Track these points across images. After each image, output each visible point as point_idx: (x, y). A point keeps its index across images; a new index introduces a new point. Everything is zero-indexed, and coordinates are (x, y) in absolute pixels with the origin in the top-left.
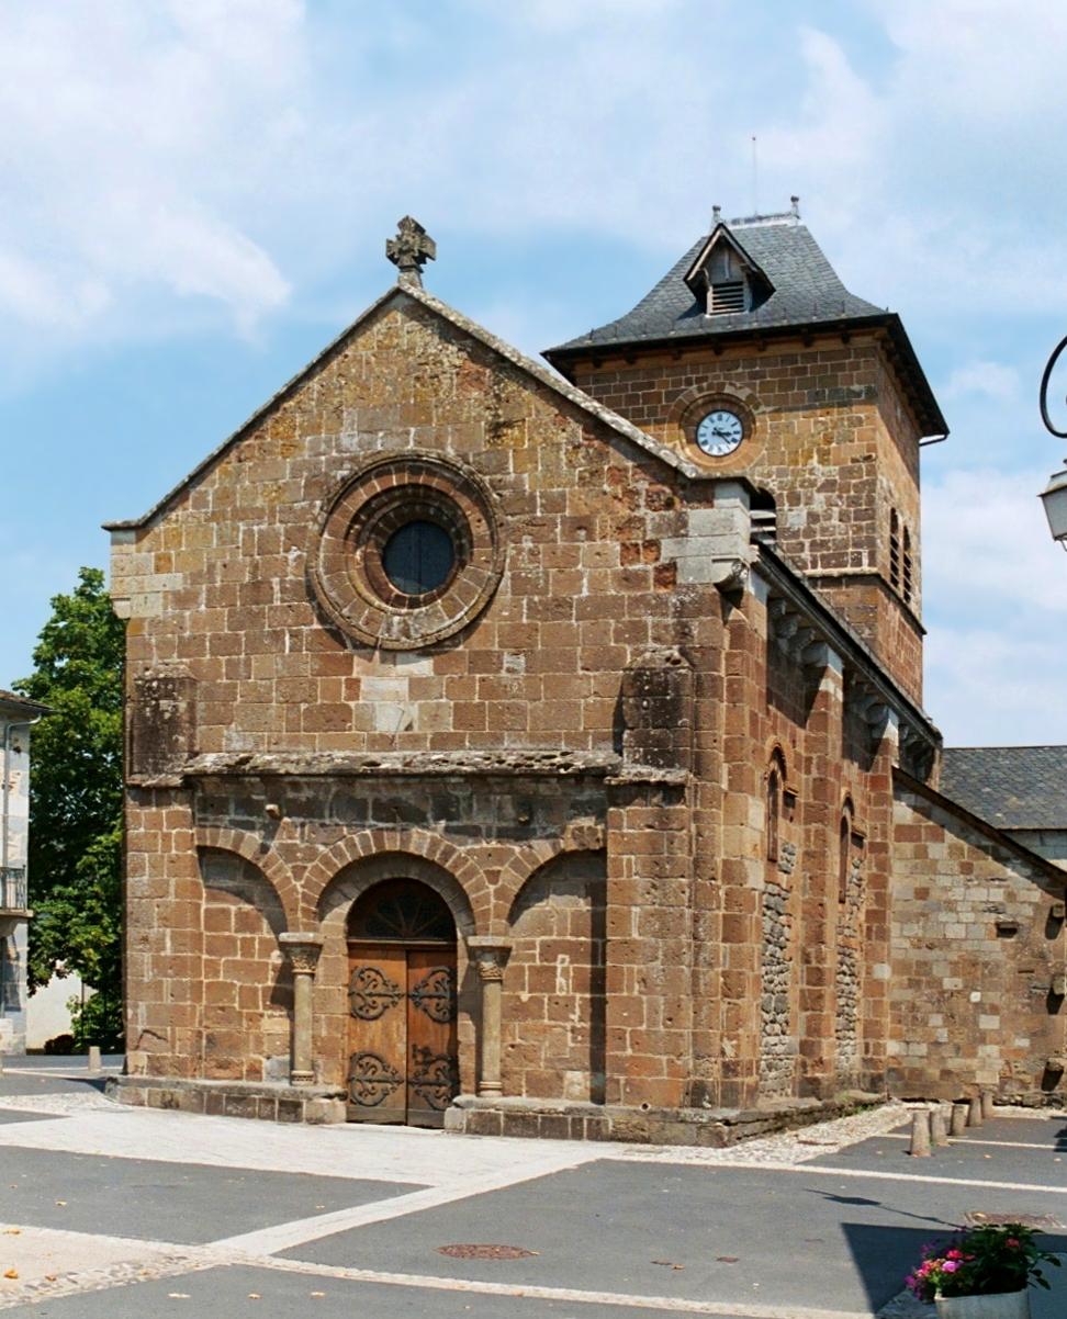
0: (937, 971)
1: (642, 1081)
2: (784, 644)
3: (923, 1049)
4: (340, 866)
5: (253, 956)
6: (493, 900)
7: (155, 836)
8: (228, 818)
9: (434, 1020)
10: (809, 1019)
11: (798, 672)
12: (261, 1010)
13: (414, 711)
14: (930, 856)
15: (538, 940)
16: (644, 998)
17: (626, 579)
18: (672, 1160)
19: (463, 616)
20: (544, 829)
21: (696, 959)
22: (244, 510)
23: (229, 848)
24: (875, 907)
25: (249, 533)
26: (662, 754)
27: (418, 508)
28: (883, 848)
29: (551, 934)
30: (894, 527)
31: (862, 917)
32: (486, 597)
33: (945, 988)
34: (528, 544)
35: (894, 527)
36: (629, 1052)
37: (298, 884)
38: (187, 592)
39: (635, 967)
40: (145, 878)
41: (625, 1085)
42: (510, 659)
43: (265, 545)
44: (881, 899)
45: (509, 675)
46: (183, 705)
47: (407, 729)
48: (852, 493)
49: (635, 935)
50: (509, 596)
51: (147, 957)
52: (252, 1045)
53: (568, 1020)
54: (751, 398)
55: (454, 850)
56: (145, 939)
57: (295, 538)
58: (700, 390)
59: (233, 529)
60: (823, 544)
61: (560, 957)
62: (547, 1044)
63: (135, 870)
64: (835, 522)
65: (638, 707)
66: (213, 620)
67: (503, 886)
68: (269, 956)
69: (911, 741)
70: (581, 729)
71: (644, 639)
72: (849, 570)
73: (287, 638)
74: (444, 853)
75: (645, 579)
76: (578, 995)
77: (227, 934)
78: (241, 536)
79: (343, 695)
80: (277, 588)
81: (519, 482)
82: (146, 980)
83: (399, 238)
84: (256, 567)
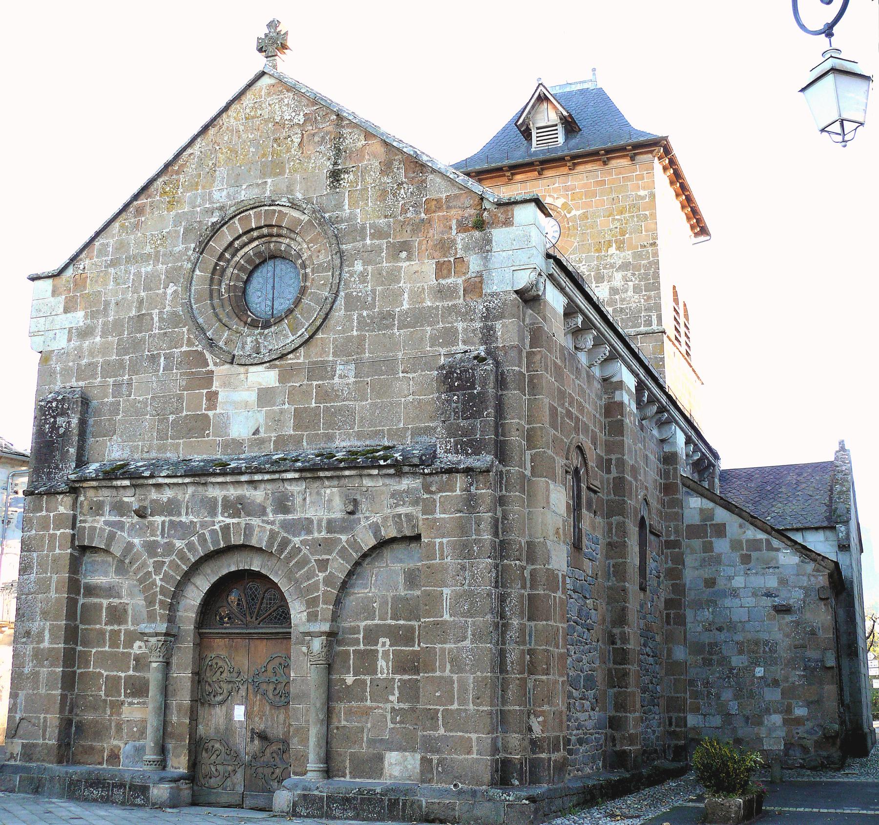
0: (726, 651)
3: (717, 721)
4: (193, 561)
6: (322, 587)
10: (616, 696)
11: (597, 385)
15: (362, 624)
19: (303, 332)
20: (367, 518)
21: (503, 638)
24: (673, 596)
25: (138, 274)
26: (470, 443)
27: (272, 245)
28: (676, 544)
30: (676, 301)
31: (662, 605)
32: (322, 314)
33: (733, 664)
34: (358, 267)
35: (676, 301)
36: (442, 731)
37: (158, 579)
38: (88, 327)
39: (447, 646)
41: (438, 764)
42: (341, 367)
43: (150, 283)
44: (679, 589)
46: (75, 421)
47: (254, 434)
48: (643, 271)
49: (447, 617)
50: (343, 312)
54: (565, 205)
55: (290, 541)
61: (381, 640)
62: (369, 725)
64: (630, 293)
66: (104, 350)
68: (132, 647)
69: (696, 458)
70: (401, 425)
71: (454, 343)
72: (643, 329)
77: (98, 626)
78: (132, 277)
80: (156, 319)
83: (266, 35)
84: (141, 302)
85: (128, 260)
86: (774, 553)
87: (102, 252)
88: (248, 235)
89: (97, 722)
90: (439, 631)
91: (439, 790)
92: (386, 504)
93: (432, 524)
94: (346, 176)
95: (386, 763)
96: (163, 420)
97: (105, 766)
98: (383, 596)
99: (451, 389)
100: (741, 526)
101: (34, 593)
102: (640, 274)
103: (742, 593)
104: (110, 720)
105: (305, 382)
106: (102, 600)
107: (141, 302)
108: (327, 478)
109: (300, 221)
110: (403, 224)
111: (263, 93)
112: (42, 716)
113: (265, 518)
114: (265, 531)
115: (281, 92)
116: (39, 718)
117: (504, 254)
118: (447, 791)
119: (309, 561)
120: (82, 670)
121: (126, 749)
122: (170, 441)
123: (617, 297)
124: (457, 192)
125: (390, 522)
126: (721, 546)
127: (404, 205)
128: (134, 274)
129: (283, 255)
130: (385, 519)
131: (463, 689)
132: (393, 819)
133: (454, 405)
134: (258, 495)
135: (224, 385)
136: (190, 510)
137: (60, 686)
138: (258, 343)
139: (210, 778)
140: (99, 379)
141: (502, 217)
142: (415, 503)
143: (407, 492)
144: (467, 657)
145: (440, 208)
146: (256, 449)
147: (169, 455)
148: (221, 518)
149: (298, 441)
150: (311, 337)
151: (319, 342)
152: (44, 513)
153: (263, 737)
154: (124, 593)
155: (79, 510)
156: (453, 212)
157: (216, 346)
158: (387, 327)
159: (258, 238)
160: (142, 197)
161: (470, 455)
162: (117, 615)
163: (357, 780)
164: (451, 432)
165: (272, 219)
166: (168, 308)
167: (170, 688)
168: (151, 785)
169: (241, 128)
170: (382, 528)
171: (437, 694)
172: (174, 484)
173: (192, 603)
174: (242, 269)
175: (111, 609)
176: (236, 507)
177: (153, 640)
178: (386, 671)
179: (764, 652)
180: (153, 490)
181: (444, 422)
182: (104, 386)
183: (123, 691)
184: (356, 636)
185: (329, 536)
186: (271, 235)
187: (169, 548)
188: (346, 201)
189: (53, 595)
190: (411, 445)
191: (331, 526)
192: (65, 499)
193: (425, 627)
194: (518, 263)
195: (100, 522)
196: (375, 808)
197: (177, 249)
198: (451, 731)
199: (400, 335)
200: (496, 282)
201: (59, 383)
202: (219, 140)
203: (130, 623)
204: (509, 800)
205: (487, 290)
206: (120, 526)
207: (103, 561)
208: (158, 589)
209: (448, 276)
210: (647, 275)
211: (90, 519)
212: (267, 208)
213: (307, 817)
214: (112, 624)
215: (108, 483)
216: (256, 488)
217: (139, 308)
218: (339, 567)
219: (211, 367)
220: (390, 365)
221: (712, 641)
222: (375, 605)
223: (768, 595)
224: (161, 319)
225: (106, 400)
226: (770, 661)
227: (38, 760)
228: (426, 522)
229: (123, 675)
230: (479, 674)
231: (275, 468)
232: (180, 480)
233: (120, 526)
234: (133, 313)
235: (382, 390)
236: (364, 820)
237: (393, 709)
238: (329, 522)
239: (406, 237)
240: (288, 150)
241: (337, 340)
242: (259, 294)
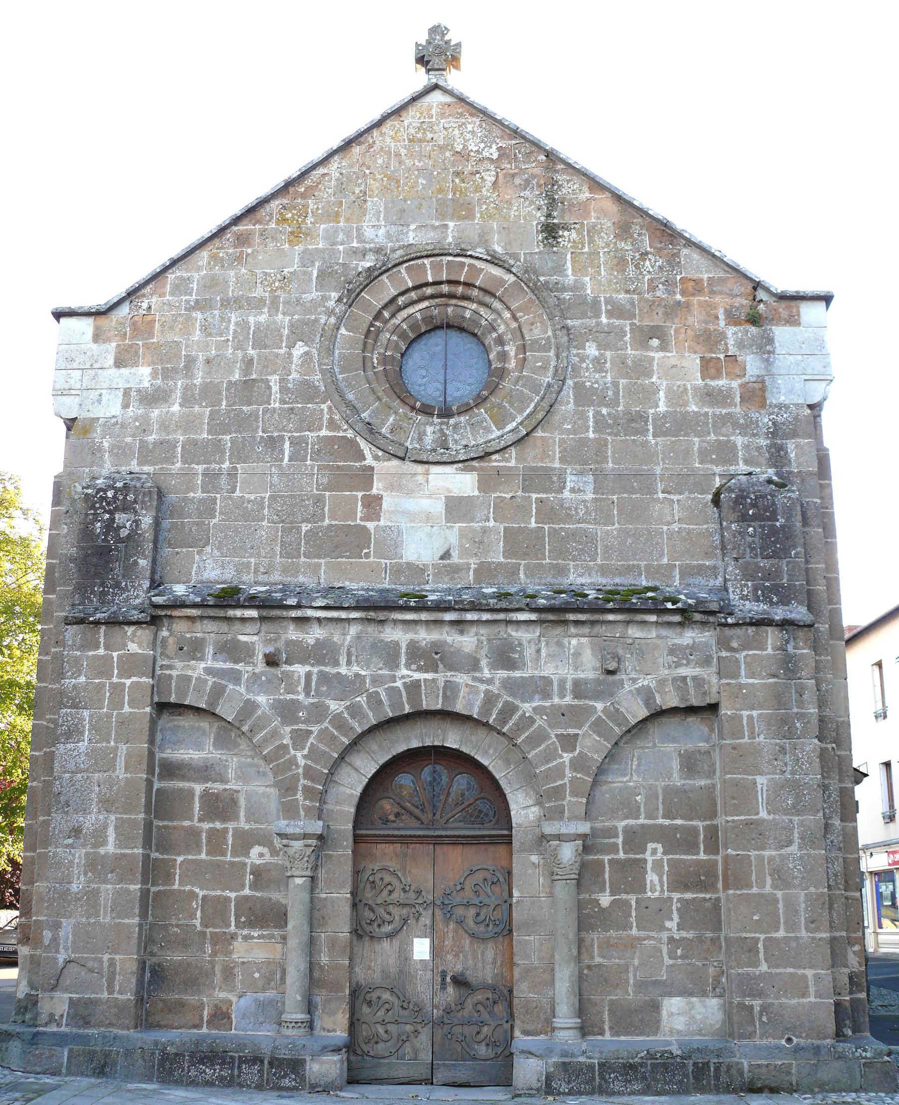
1: (780, 1005)
5: (223, 854)
6: (569, 774)
7: (101, 686)
8: (203, 665)
9: (473, 936)
13: (452, 536)
15: (621, 825)
16: (779, 894)
17: (708, 394)
20: (634, 680)
22: (237, 300)
25: (243, 325)
27: (450, 310)
29: (637, 818)
32: (545, 405)
34: (592, 350)
36: (764, 967)
37: (300, 756)
39: (766, 853)
40: (83, 746)
42: (574, 478)
43: (264, 337)
46: (147, 521)
47: (442, 558)
49: (763, 814)
50: (571, 406)
51: (79, 855)
53: (663, 928)
55: (515, 708)
56: (76, 832)
59: (222, 319)
61: (650, 846)
62: (636, 962)
65: (742, 534)
66: (188, 424)
67: (581, 752)
68: (247, 854)
71: (733, 461)
73: (287, 445)
74: (501, 712)
76: (676, 896)
77: (187, 823)
78: (232, 327)
79: (359, 515)
80: (275, 388)
84: (248, 363)
85: (226, 303)
88: (419, 292)
89: (189, 964)
91: (768, 1048)
92: (661, 662)
94: (566, 233)
95: (664, 1013)
96: (291, 529)
97: (205, 1030)
98: (651, 787)
99: (744, 518)
101: (86, 770)
106: (193, 785)
107: (248, 363)
108: (577, 623)
109: (502, 282)
110: (652, 304)
111: (433, 112)
112: (106, 957)
113: (478, 675)
115: (461, 115)
116: (101, 961)
117: (791, 358)
118: (779, 1048)
119: (547, 737)
120: (161, 888)
121: (240, 1003)
122: (303, 559)
124: (722, 274)
125: (669, 688)
127: (651, 281)
128: (237, 324)
129: (465, 325)
130: (662, 682)
131: (791, 908)
132: (702, 1090)
133: (750, 539)
134: (467, 642)
135: (391, 487)
136: (353, 658)
137: (137, 911)
138: (445, 435)
139: (377, 1043)
140: (178, 465)
141: (784, 314)
142: (706, 662)
143: (693, 647)
144: (795, 867)
145: (700, 291)
146: (446, 580)
147: (301, 579)
148: (405, 672)
149: (513, 572)
150: (527, 435)
151: (539, 443)
152: (101, 651)
153: (460, 982)
154: (231, 774)
155: (159, 650)
156: (717, 299)
157: (380, 434)
158: (637, 432)
159: (432, 297)
160: (245, 221)
161: (777, 604)
162: (220, 807)
163: (623, 1038)
164: (748, 573)
166: (294, 375)
167: (317, 915)
168: (308, 1058)
169: (403, 152)
170: (657, 696)
171: (756, 918)
172: (326, 619)
173: (348, 791)
174: (403, 335)
176: (429, 657)
177: (297, 845)
178: (658, 888)
180: (292, 627)
181: (736, 559)
183: (233, 919)
184: (612, 840)
185: (576, 702)
186: (451, 296)
187: (318, 712)
188: (569, 264)
189: (120, 773)
190: (702, 589)
191: (580, 689)
192: (139, 633)
193: (733, 828)
194: (810, 371)
195: (198, 669)
196: (674, 1075)
197: (307, 297)
198: (777, 966)
199: (657, 444)
200: (783, 391)
201: (108, 465)
202: (368, 161)
204: (866, 1058)
205: (771, 400)
206: (235, 677)
207: (193, 728)
208: (300, 771)
209: (718, 376)
211: (179, 664)
212: (450, 258)
213: (570, 1093)
214: (212, 820)
215: (221, 613)
216: (462, 632)
218: (593, 746)
219: (369, 461)
220: (646, 482)
222: (638, 798)
224: (283, 389)
225: (192, 494)
227: (100, 1024)
228: (727, 688)
230: (812, 890)
231: (504, 604)
232: (343, 615)
233: (235, 677)
234: (236, 376)
236: (658, 1094)
237: (671, 940)
238: (577, 683)
239: (657, 321)
240: (478, 189)
241: (565, 442)
242: (424, 372)
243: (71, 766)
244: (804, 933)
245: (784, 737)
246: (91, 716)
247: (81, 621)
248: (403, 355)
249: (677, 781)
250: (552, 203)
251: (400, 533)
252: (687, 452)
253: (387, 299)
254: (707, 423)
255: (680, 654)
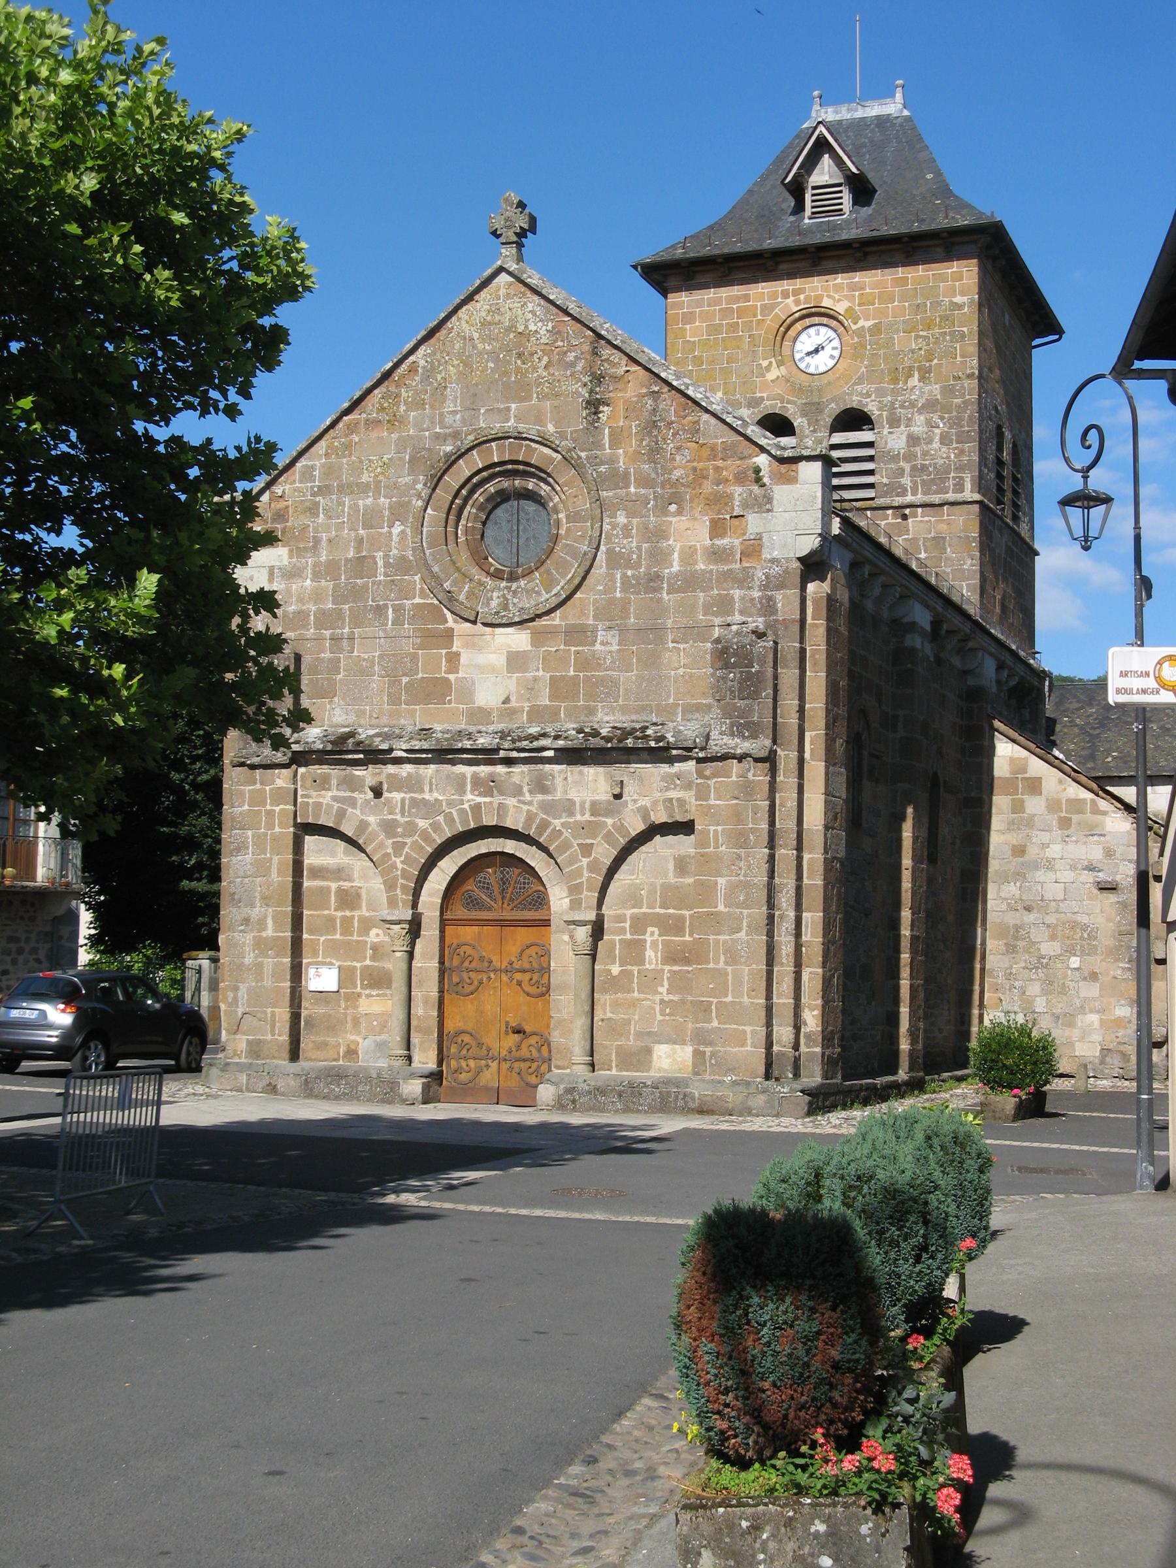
2: (869, 605)
6: (586, 874)
8: (330, 794)
12: (359, 989)
14: (1028, 811)
15: (629, 913)
16: (729, 969)
18: (756, 1128)
19: (560, 589)
20: (635, 801)
22: (349, 486)
23: (331, 825)
25: (355, 508)
26: (748, 725)
34: (622, 519)
36: (715, 1024)
37: (398, 861)
39: (721, 937)
43: (371, 519)
45: (603, 648)
49: (721, 908)
50: (604, 569)
52: (349, 1025)
53: (657, 992)
56: (247, 921)
57: (398, 513)
58: (797, 302)
60: (924, 468)
61: (650, 929)
62: (636, 1017)
63: (238, 850)
64: (936, 444)
66: (317, 596)
71: (730, 612)
72: (950, 496)
73: (390, 611)
75: (732, 554)
77: (326, 912)
80: (380, 563)
81: (613, 460)
82: (247, 961)
84: (360, 541)
85: (341, 489)
86: (1100, 817)
87: (308, 475)
90: (715, 922)
93: (706, 811)
94: (606, 409)
96: (394, 682)
98: (652, 884)
100: (1060, 782)
102: (950, 418)
103: (1058, 865)
104: (345, 1014)
105: (562, 647)
107: (360, 541)
112: (269, 1010)
114: (521, 811)
117: (786, 515)
121: (365, 1045)
123: (918, 449)
125: (661, 807)
126: (1035, 805)
128: (350, 507)
130: (655, 803)
133: (730, 683)
135: (467, 645)
138: (507, 600)
142: (688, 786)
148: (470, 797)
149: (555, 713)
152: (258, 786)
154: (356, 876)
157: (457, 600)
158: (655, 590)
162: (349, 899)
164: (727, 714)
165: (518, 453)
166: (395, 552)
169: (476, 335)
175: (340, 892)
177: (396, 928)
179: (1082, 938)
182: (319, 639)
185: (593, 819)
187: (411, 828)
189: (274, 876)
191: (595, 808)
195: (327, 797)
198: (725, 1023)
199: (669, 600)
203: (364, 908)
205: (766, 555)
206: (353, 803)
209: (722, 535)
210: (960, 419)
214: (343, 910)
217: (358, 549)
218: (605, 853)
221: (1019, 923)
223: (1091, 868)
224: (387, 565)
226: (1088, 951)
229: (358, 965)
230: (754, 966)
233: (353, 803)
234: (351, 554)
235: (652, 661)
238: (594, 804)
240: (535, 369)
243: (241, 873)
244: (746, 999)
245: (741, 847)
246: (253, 836)
247: (242, 764)
248: (484, 523)
249: (672, 879)
250: (598, 379)
251: (473, 683)
252: (693, 607)
253: (463, 480)
254: (711, 580)
255: (670, 780)
